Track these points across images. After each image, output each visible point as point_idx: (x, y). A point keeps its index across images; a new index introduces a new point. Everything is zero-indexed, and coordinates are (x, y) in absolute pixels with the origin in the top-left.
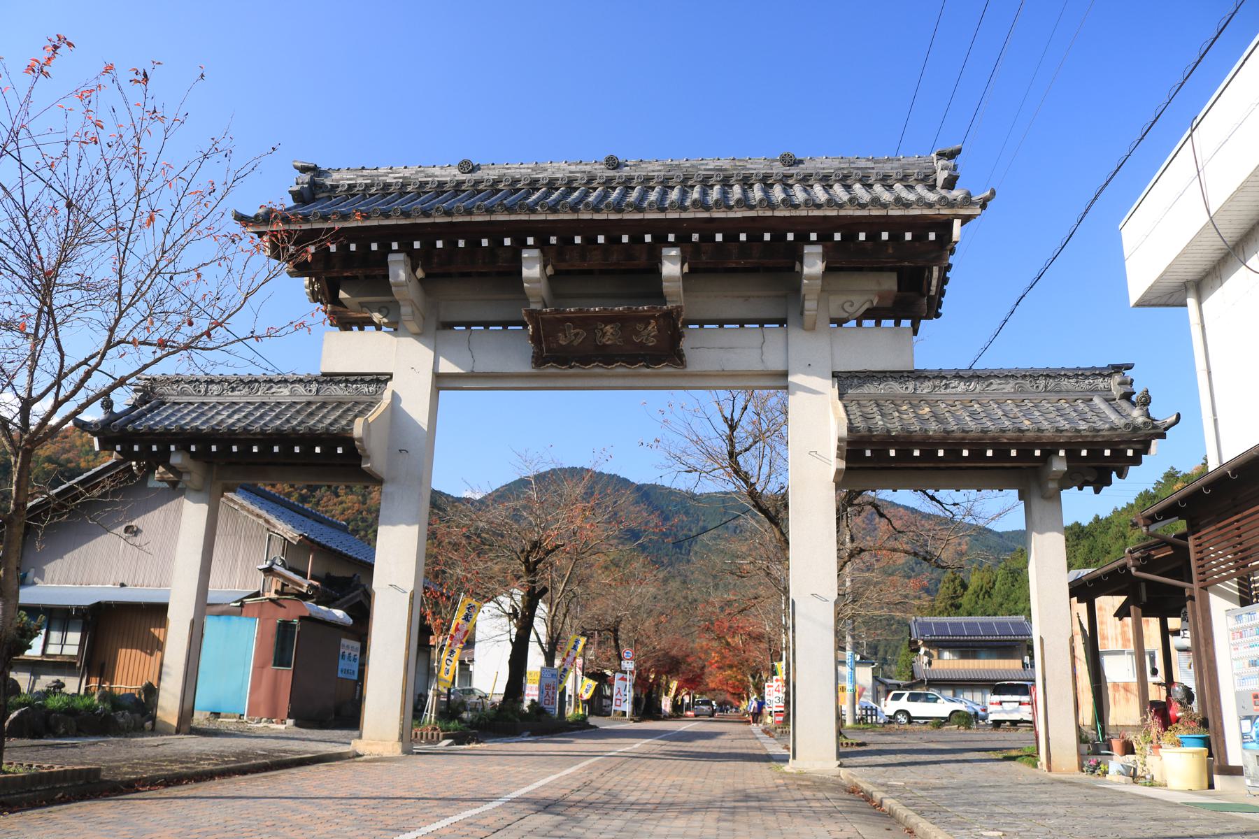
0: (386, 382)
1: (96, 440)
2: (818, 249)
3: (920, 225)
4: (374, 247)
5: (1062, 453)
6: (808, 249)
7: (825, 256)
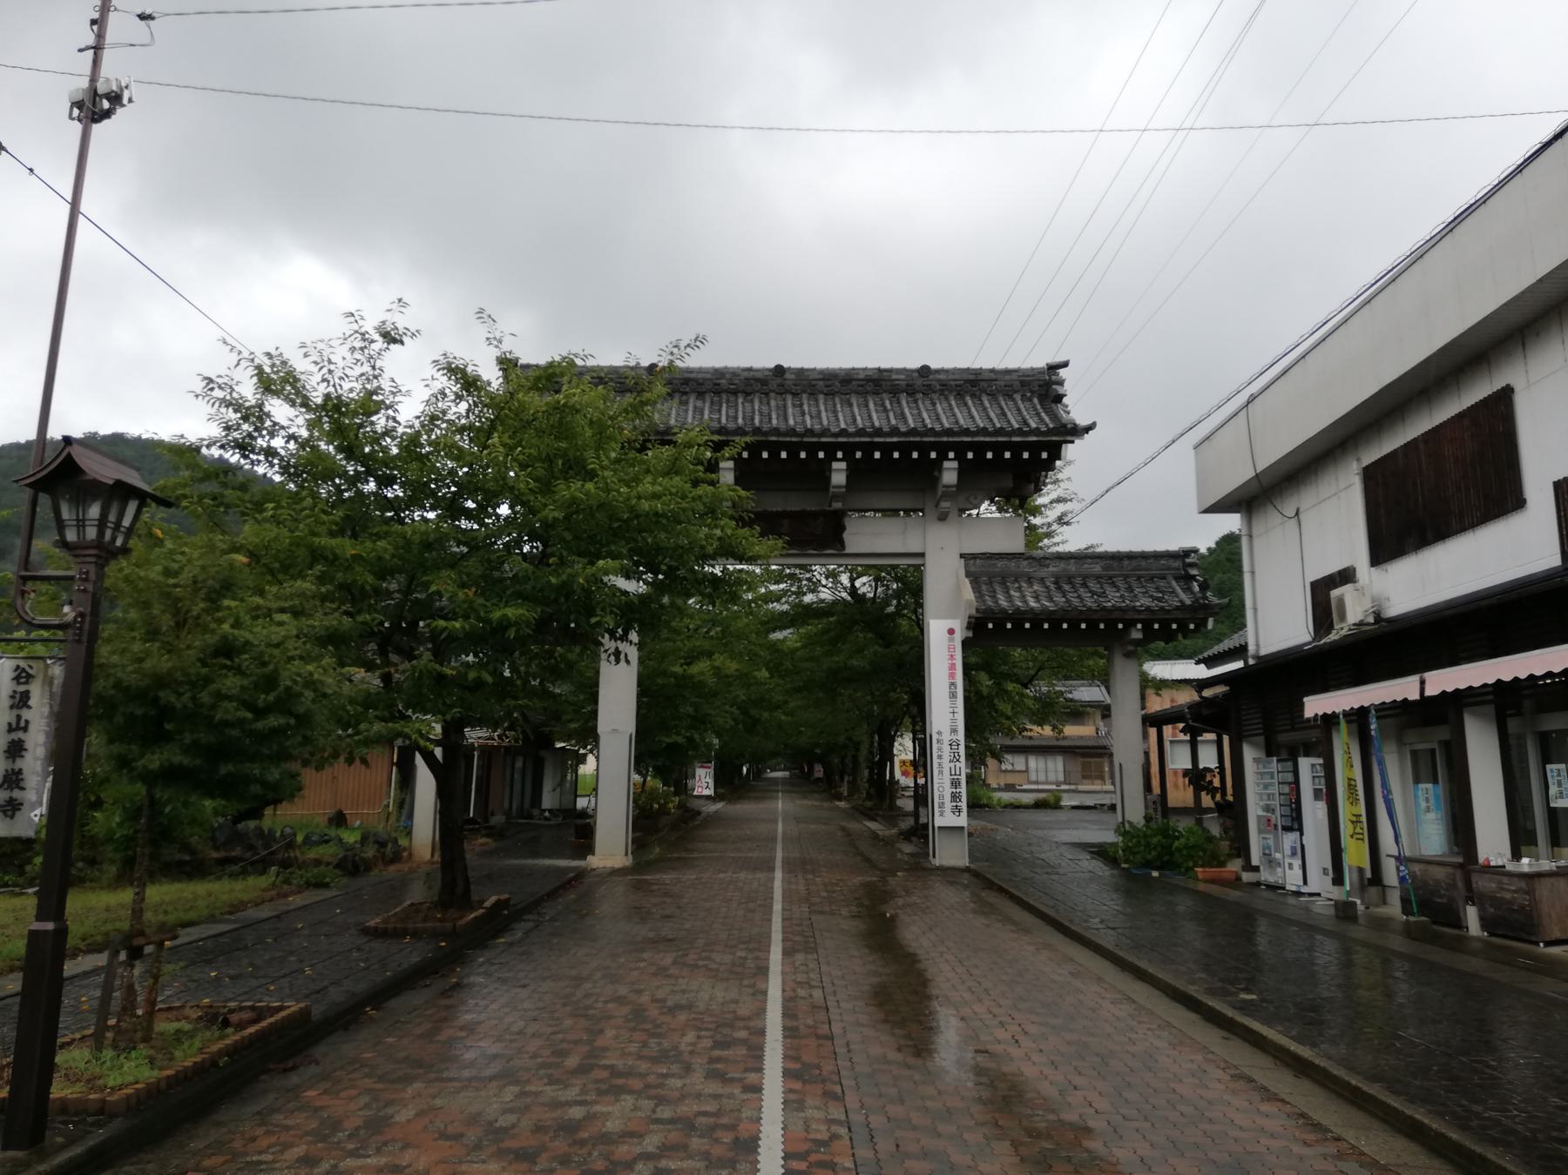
5: (1139, 626)
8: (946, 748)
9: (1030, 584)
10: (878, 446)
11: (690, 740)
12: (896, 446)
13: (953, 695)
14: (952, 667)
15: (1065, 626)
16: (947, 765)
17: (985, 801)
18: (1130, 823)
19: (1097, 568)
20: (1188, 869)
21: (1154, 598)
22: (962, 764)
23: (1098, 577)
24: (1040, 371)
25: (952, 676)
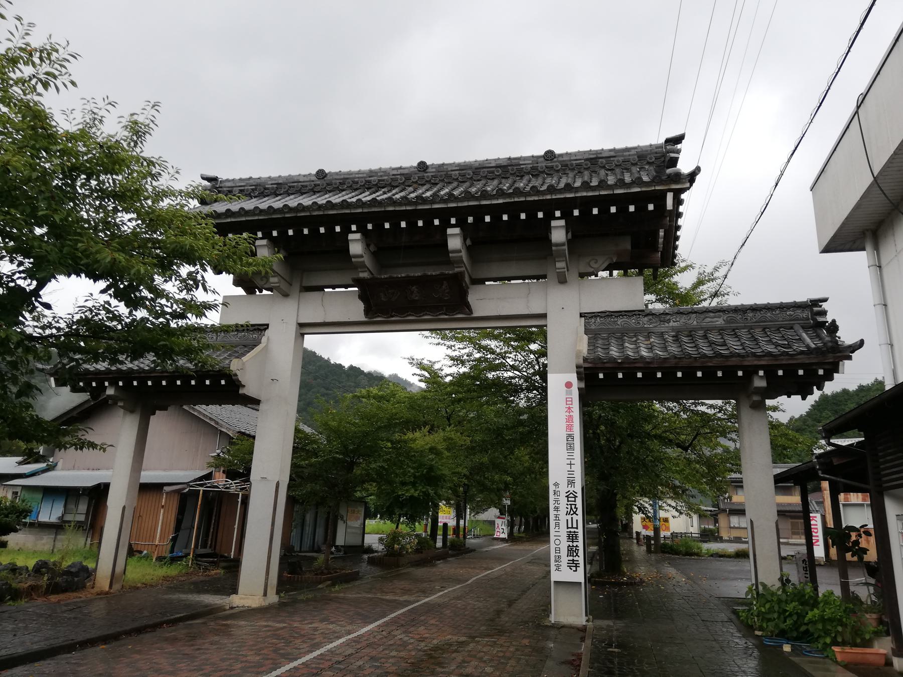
0: (265, 329)
1: (52, 379)
2: (562, 223)
3: (640, 199)
4: (338, 229)
5: (761, 373)
6: (554, 223)
7: (568, 228)
8: (563, 500)
9: (648, 338)
10: (489, 209)
11: (426, 494)
12: (504, 208)
13: (570, 447)
14: (570, 419)
15: (679, 374)
16: (563, 518)
17: (696, 550)
18: (764, 586)
19: (720, 322)
20: (826, 646)
21: (777, 345)
22: (579, 517)
23: (721, 330)
24: (659, 147)
25: (569, 427)
